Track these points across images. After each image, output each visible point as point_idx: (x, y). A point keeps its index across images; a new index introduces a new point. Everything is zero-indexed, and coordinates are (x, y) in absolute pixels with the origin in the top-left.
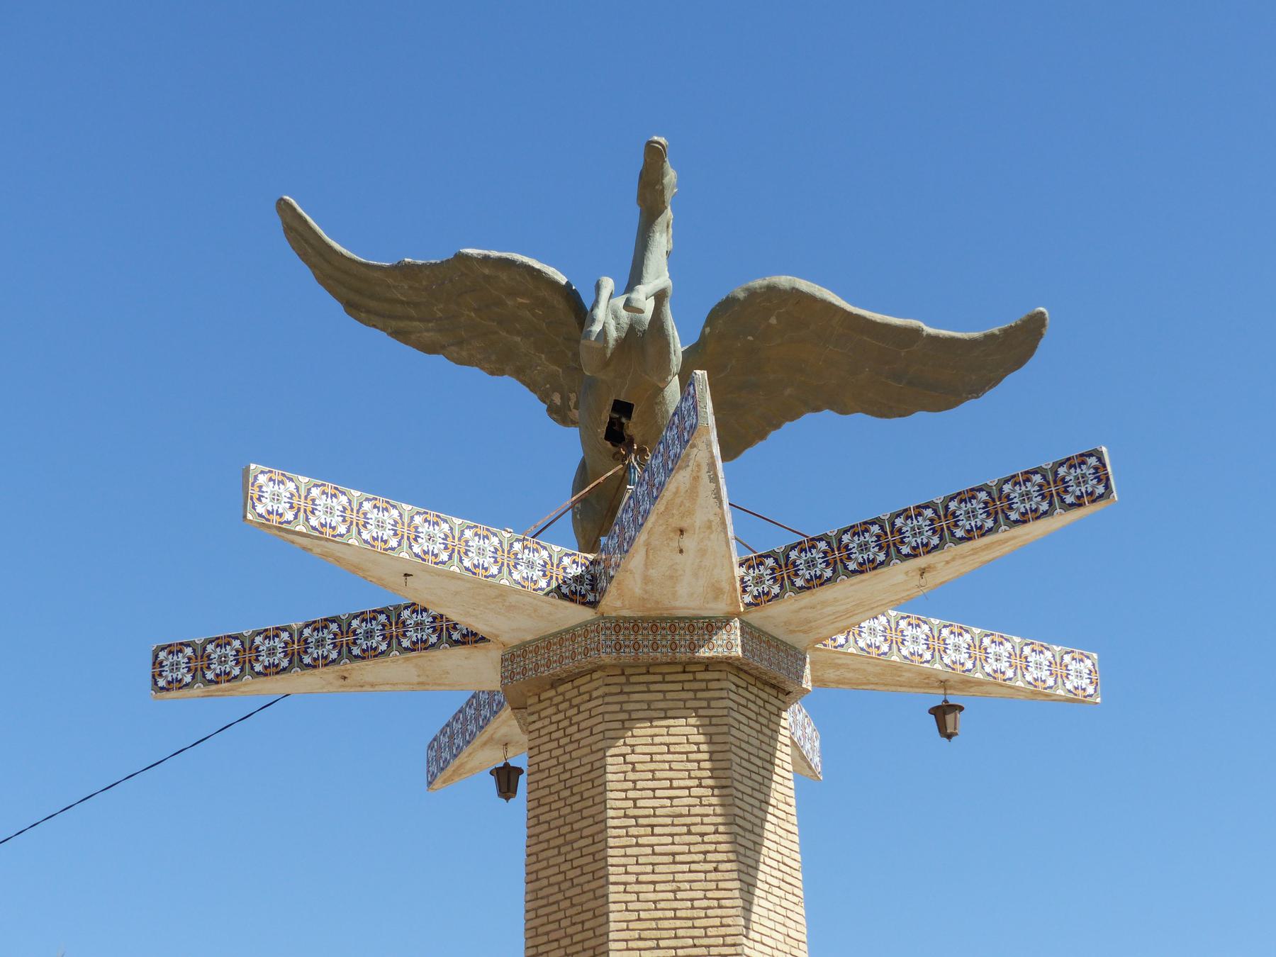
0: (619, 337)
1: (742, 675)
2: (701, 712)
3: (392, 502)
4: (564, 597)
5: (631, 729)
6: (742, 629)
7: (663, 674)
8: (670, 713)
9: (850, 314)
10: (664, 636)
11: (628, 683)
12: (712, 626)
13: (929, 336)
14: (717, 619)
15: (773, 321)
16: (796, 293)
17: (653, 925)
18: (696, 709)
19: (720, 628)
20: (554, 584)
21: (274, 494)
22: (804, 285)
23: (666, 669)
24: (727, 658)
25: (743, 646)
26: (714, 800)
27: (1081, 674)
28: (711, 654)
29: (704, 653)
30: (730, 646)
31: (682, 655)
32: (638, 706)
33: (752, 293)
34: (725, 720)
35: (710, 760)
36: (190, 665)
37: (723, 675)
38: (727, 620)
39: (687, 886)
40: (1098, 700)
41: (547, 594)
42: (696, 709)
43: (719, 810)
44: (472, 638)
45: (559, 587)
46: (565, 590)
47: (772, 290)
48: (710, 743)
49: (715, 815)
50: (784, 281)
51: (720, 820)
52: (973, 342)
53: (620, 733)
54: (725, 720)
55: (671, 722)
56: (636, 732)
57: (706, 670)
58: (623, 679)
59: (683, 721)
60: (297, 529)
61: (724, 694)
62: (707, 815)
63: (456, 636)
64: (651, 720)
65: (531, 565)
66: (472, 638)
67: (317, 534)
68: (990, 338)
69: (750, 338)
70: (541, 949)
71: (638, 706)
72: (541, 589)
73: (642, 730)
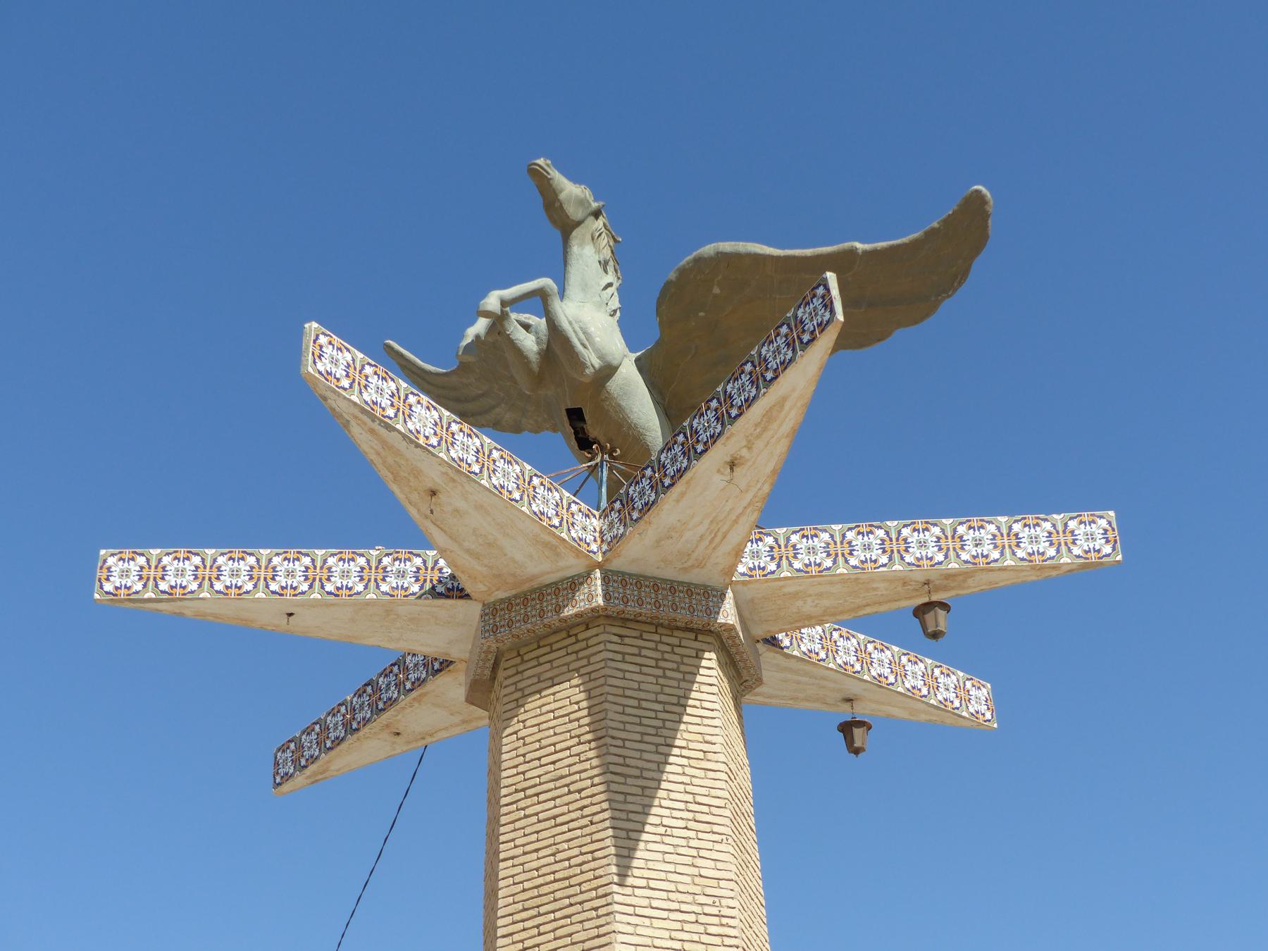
0: (541, 350)
1: (629, 625)
2: (583, 671)
3: (248, 550)
4: (441, 595)
5: (523, 706)
6: (603, 579)
7: (551, 645)
8: (556, 681)
9: (778, 258)
10: (533, 607)
11: (523, 662)
12: (575, 583)
13: (865, 252)
14: (579, 576)
15: (716, 290)
16: (722, 257)
17: (535, 892)
18: (577, 670)
19: (582, 584)
20: (428, 586)
21: (121, 572)
22: (727, 246)
23: (552, 639)
24: (593, 610)
25: (605, 596)
26: (591, 754)
27: (1092, 536)
28: (575, 610)
29: (568, 612)
30: (591, 597)
31: (551, 619)
32: (530, 682)
33: (683, 272)
34: (603, 672)
35: (589, 715)
36: (296, 756)
37: (601, 629)
38: (588, 575)
39: (565, 846)
40: (1119, 558)
41: (420, 597)
42: (577, 670)
43: (595, 762)
44: (446, 664)
45: (433, 588)
46: (440, 589)
47: (698, 261)
48: (589, 698)
49: (592, 768)
50: (709, 249)
51: (596, 772)
52: (915, 244)
53: (513, 713)
54: (603, 672)
55: (557, 688)
56: (527, 707)
57: (588, 628)
58: (518, 660)
59: (567, 685)
60: (146, 596)
61: (601, 647)
62: (585, 770)
63: (437, 666)
64: (539, 692)
65: (401, 574)
66: (446, 664)
67: (166, 596)
68: (931, 233)
69: (702, 314)
70: (528, 943)
71: (530, 682)
72: (414, 594)
73: (533, 704)
